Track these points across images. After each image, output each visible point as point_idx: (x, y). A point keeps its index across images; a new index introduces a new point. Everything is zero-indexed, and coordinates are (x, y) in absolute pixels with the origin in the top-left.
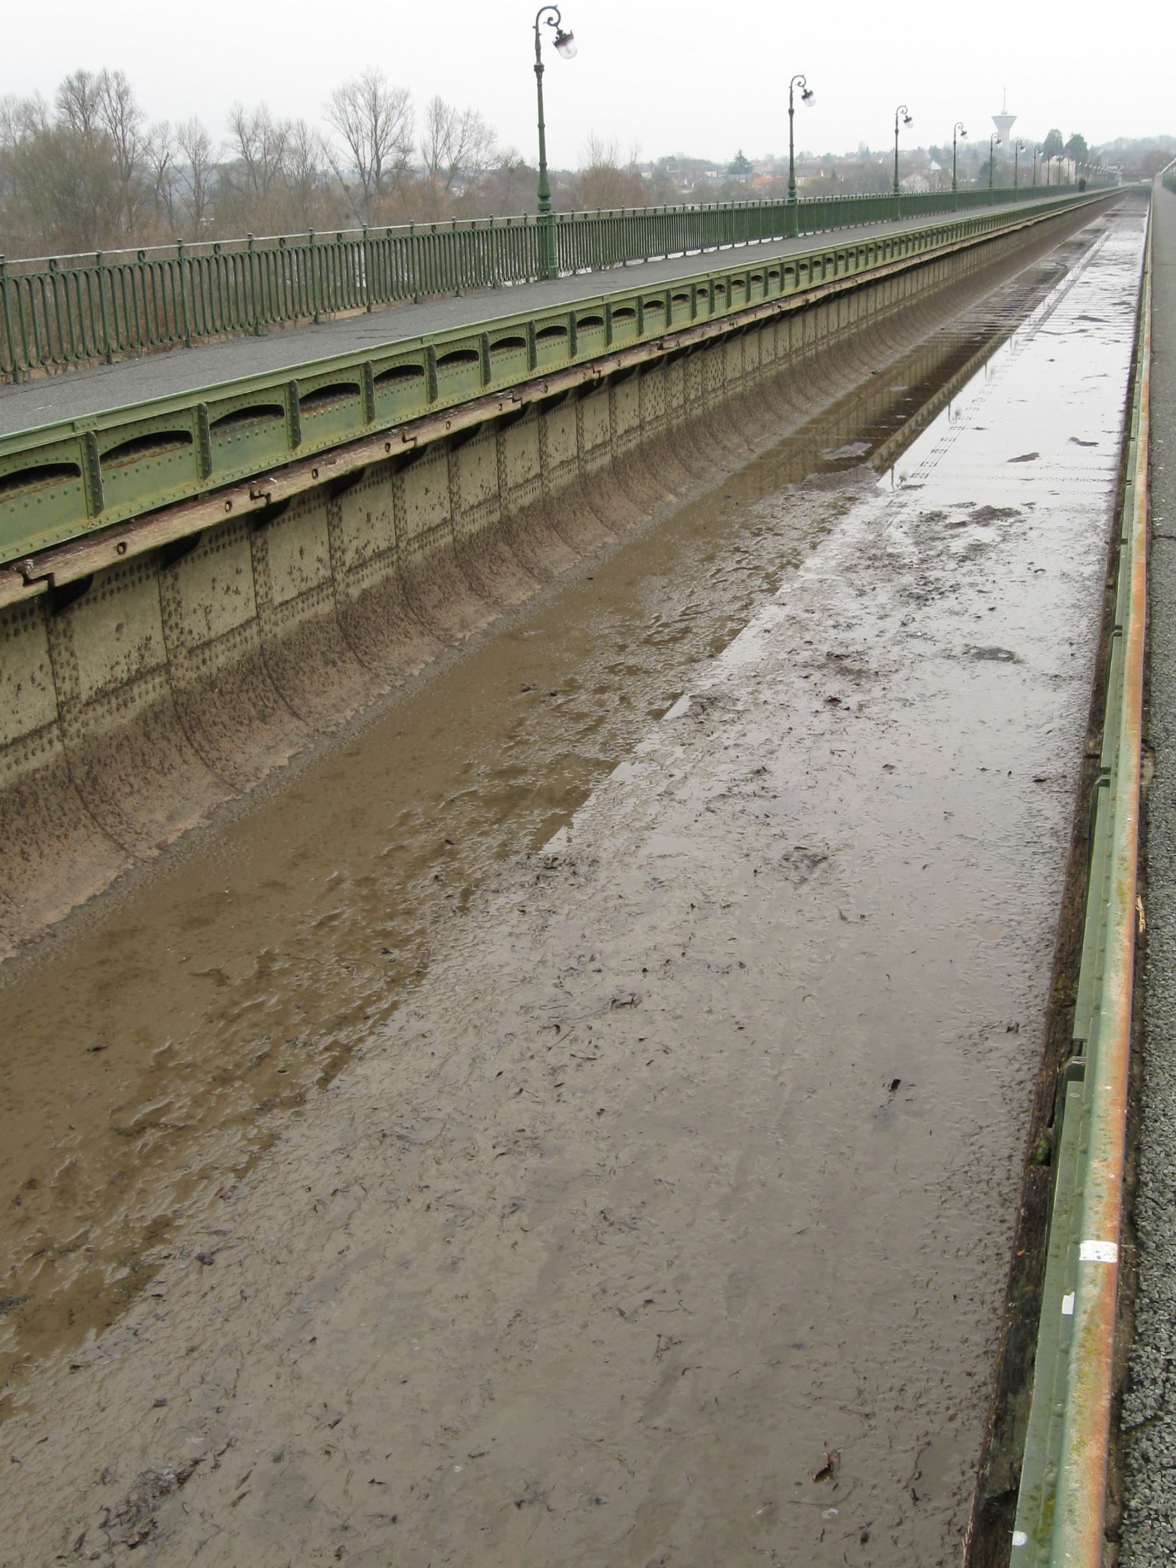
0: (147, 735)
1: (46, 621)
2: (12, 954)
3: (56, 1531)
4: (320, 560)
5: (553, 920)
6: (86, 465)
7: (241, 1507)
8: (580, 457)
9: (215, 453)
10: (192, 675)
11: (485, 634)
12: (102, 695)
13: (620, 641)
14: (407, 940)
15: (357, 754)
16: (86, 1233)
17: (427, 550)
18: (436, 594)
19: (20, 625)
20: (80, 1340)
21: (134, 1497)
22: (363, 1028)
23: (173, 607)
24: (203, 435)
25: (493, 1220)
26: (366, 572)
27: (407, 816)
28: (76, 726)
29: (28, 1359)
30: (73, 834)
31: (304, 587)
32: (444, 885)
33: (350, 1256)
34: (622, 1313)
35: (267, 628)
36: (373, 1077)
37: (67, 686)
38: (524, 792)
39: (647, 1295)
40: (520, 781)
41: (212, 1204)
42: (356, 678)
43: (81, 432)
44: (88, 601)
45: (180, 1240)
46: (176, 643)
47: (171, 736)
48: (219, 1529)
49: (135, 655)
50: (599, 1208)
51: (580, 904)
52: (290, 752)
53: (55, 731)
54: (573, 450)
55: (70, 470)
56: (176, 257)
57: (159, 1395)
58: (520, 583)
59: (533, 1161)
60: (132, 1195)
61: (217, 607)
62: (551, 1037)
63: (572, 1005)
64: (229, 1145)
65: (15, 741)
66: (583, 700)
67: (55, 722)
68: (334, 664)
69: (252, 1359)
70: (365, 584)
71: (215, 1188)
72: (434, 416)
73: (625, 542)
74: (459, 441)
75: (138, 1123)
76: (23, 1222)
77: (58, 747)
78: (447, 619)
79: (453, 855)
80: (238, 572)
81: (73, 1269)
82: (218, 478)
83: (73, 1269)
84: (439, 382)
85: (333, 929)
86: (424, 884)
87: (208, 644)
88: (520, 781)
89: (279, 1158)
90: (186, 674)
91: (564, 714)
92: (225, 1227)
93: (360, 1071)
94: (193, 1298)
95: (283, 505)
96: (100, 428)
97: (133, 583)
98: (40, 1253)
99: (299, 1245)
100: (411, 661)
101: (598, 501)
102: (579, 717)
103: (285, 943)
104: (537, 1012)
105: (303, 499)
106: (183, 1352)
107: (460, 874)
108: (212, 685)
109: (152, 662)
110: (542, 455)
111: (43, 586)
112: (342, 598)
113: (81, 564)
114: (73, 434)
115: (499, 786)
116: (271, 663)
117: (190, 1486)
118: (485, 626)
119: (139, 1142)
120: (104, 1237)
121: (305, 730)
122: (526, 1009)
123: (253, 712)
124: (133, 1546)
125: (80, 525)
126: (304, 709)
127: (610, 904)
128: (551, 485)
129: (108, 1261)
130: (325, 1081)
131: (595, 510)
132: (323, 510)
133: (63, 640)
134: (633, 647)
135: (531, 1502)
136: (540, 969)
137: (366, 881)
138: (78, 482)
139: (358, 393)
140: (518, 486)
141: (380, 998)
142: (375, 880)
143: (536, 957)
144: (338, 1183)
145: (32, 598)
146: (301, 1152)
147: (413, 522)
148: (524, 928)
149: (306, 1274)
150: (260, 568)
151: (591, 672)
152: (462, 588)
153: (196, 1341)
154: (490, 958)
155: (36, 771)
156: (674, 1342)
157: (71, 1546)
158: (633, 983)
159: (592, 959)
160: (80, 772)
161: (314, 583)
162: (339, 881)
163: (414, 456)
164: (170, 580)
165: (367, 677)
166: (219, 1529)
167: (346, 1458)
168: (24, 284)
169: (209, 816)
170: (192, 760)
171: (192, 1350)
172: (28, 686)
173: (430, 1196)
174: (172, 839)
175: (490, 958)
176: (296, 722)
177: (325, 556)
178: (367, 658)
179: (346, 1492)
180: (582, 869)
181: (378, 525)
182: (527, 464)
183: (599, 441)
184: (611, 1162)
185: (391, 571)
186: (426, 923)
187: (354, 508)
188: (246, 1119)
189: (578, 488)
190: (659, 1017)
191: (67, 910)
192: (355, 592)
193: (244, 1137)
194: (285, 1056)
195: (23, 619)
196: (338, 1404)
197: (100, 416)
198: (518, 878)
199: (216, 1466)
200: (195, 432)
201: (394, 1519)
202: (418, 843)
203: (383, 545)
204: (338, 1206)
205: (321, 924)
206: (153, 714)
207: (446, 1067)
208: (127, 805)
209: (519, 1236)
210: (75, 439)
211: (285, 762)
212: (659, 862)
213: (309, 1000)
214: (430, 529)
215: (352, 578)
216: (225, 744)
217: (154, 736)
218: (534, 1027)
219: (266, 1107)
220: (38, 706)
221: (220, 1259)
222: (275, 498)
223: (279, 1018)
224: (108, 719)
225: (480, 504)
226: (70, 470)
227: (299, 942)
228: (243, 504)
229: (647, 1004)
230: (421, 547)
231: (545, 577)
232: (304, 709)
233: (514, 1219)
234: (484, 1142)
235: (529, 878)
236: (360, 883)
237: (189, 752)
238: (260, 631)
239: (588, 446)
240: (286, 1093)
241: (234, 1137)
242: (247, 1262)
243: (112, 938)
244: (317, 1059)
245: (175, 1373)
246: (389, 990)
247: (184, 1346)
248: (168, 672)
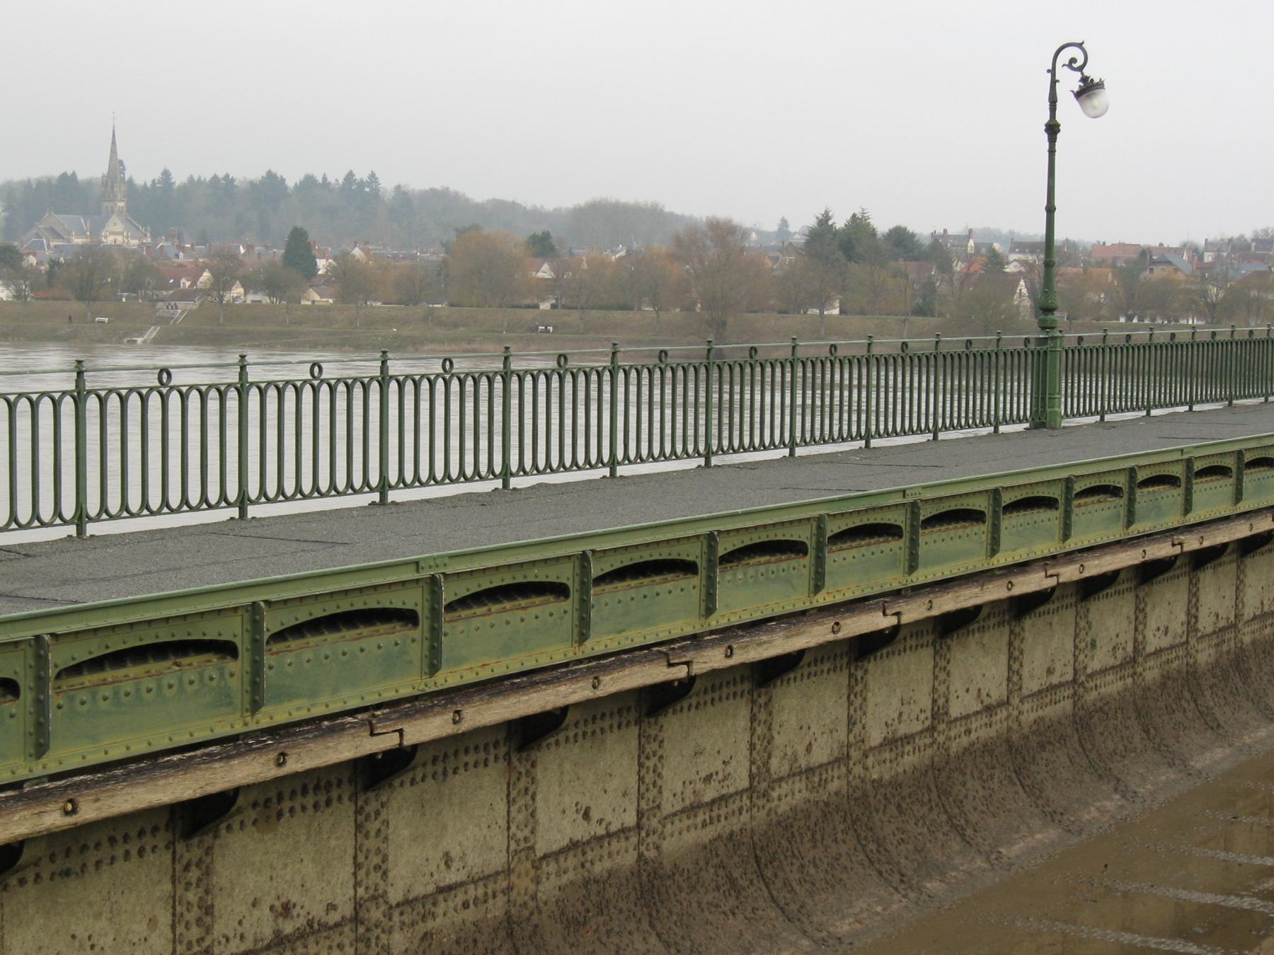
1: (354, 797)
24: (820, 548)
43: (425, 574)
46: (651, 805)
56: (865, 353)
67: (747, 790)
72: (1069, 557)
74: (1202, 559)
84: (1074, 517)
96: (449, 571)
97: (602, 730)
114: (417, 576)
125: (1117, 533)
132: (634, 731)
139: (901, 536)
163: (1105, 582)
168: (986, 355)
197: (924, 488)
200: (573, 586)
210: (417, 581)
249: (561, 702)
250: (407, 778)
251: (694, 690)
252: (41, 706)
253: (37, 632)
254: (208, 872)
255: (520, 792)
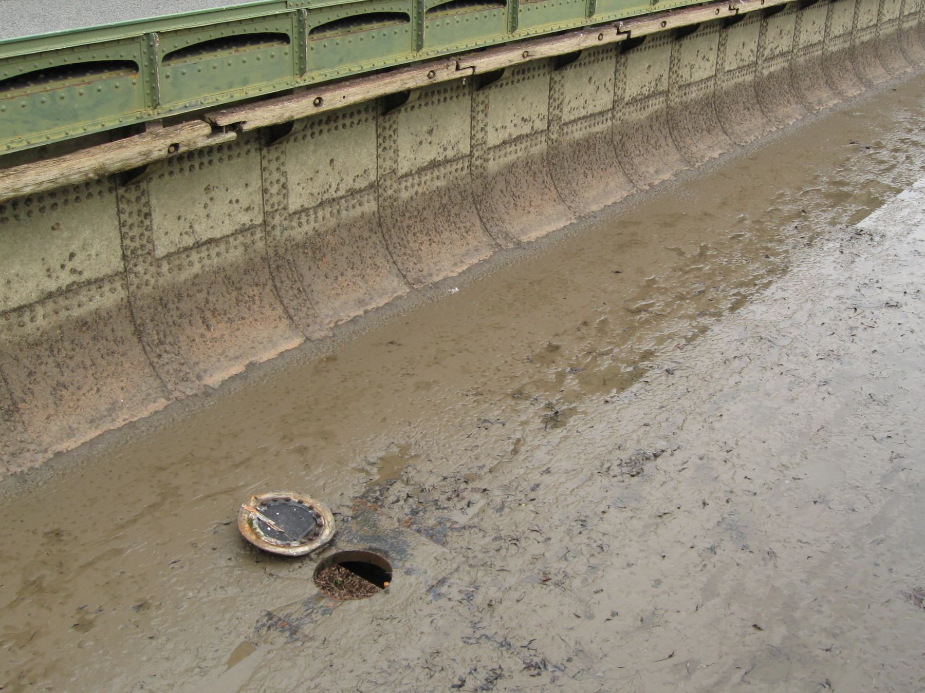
0: (651, 126)
1: (617, 56)
2: (575, 221)
3: (598, 463)
4: (752, 51)
5: (857, 260)
6: (296, 35)
7: (683, 472)
8: (901, 18)
9: (163, 85)
10: (678, 100)
11: (831, 110)
12: (634, 101)
13: (909, 126)
14: (779, 254)
15: (756, 158)
16: (612, 350)
17: (807, 57)
18: (808, 83)
19: (605, 56)
20: (609, 392)
21: (633, 458)
22: (753, 290)
23: (676, 61)
24: (420, 15)
25: (814, 386)
26: (774, 62)
27: (782, 194)
28: (620, 114)
29: (584, 394)
30: (609, 169)
31: (741, 64)
32: (799, 232)
33: (741, 386)
34: (875, 439)
35: (719, 83)
36: (757, 311)
37: (619, 93)
38: (848, 195)
39: (889, 434)
40: (845, 189)
41: (673, 350)
42: (759, 120)
44: (496, 86)
45: (658, 361)
47: (663, 131)
48: (672, 479)
49: (653, 83)
50: (868, 392)
51: (873, 255)
52: (720, 152)
53: (610, 115)
54: (897, 14)
55: (283, 38)
57: (646, 421)
58: (854, 85)
59: (837, 365)
60: (634, 339)
61: (697, 66)
62: (851, 313)
63: (864, 301)
64: (683, 327)
65: (591, 115)
66: (884, 154)
68: (749, 109)
69: (690, 417)
70: (772, 69)
71: (676, 343)
73: (917, 73)
75: (637, 308)
76: (582, 338)
77: (609, 123)
78: (812, 97)
79: (806, 218)
80: (711, 49)
81: (605, 364)
82: (429, 51)
83: (605, 364)
85: (740, 241)
86: (789, 229)
87: (689, 85)
88: (845, 189)
89: (707, 337)
90: (675, 99)
91: (873, 159)
92: (680, 361)
93: (751, 308)
94: (663, 387)
95: (640, 40)
96: (311, 7)
98: (590, 353)
99: (716, 375)
100: (788, 117)
101: (905, 47)
102: (882, 162)
103: (714, 243)
104: (844, 300)
105: (656, 37)
106: (658, 407)
107: (809, 228)
108: (687, 107)
109: (661, 89)
110: (880, 13)
111: (625, 36)
112: (758, 74)
113: (644, 28)
115: (834, 189)
116: (717, 102)
117: (659, 460)
118: (831, 105)
119: (635, 318)
120: (621, 351)
121: (729, 142)
122: (840, 298)
123: (704, 127)
124: (633, 476)
126: (730, 131)
127: (890, 258)
128: (881, 32)
129: (623, 362)
130: (733, 309)
131: (903, 52)
133: (622, 68)
134: (916, 131)
135: (821, 503)
136: (849, 281)
137: (758, 222)
138: (406, 26)
140: (863, 29)
141: (762, 277)
142: (763, 223)
143: (847, 275)
144: (737, 354)
145: (618, 43)
146: (719, 337)
147: (803, 39)
148: (840, 260)
149: (719, 388)
150: (722, 49)
151: (890, 140)
152: (822, 82)
153: (664, 404)
154: (822, 271)
155: (597, 133)
156: (899, 456)
157: (604, 470)
158: (898, 297)
159: (877, 282)
160: (617, 138)
161: (746, 63)
162: (743, 219)
164: (677, 47)
165: (765, 121)
166: (672, 479)
167: (734, 465)
169: (676, 175)
170: (671, 145)
171: (663, 407)
172: (602, 88)
173: (782, 369)
174: (656, 183)
175: (822, 271)
176: (724, 137)
177: (755, 50)
178: (765, 110)
179: (733, 478)
180: (877, 238)
181: (785, 37)
182: (870, 17)
183: (913, 11)
184: (877, 374)
185: (786, 65)
186: (789, 248)
187: (689, 48)
188: (692, 317)
189: (895, 37)
190: (910, 316)
191: (602, 206)
192: (766, 73)
193: (690, 325)
194: (712, 293)
195: (335, 121)
196: (731, 443)
198: (840, 235)
199: (672, 455)
201: (755, 494)
202: (787, 209)
203: (785, 49)
204: (736, 364)
205: (733, 238)
206: (655, 117)
207: (795, 315)
208: (637, 161)
209: (827, 396)
210: (287, 14)
211: (717, 156)
212: (920, 243)
213: (726, 272)
214: (811, 45)
215: (766, 64)
216: (688, 140)
217: (654, 128)
218: (843, 307)
219: (702, 314)
220: (604, 100)
221: (677, 373)
222: (740, 12)
223: (711, 276)
224: (634, 115)
225: (840, 36)
226: (283, 38)
227: (721, 244)
228: (611, 36)
229: (904, 308)
230: (804, 54)
231: (869, 84)
232: (730, 131)
233: (825, 388)
234: (812, 352)
235: (847, 237)
236: (754, 222)
237: (670, 141)
238: (715, 83)
239: (906, 13)
240: (712, 310)
241: (685, 324)
242: (690, 377)
243: (624, 224)
244: (729, 298)
245: (654, 415)
246: (768, 275)
247: (659, 405)
248: (667, 96)
249: (576, 49)
250: (695, 34)
251: (503, 76)
252: (420, 26)
253: (148, 31)
254: (486, 106)
255: (383, 141)
